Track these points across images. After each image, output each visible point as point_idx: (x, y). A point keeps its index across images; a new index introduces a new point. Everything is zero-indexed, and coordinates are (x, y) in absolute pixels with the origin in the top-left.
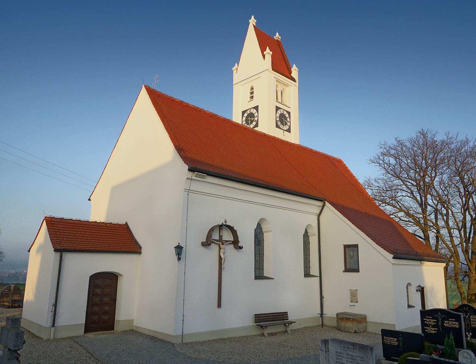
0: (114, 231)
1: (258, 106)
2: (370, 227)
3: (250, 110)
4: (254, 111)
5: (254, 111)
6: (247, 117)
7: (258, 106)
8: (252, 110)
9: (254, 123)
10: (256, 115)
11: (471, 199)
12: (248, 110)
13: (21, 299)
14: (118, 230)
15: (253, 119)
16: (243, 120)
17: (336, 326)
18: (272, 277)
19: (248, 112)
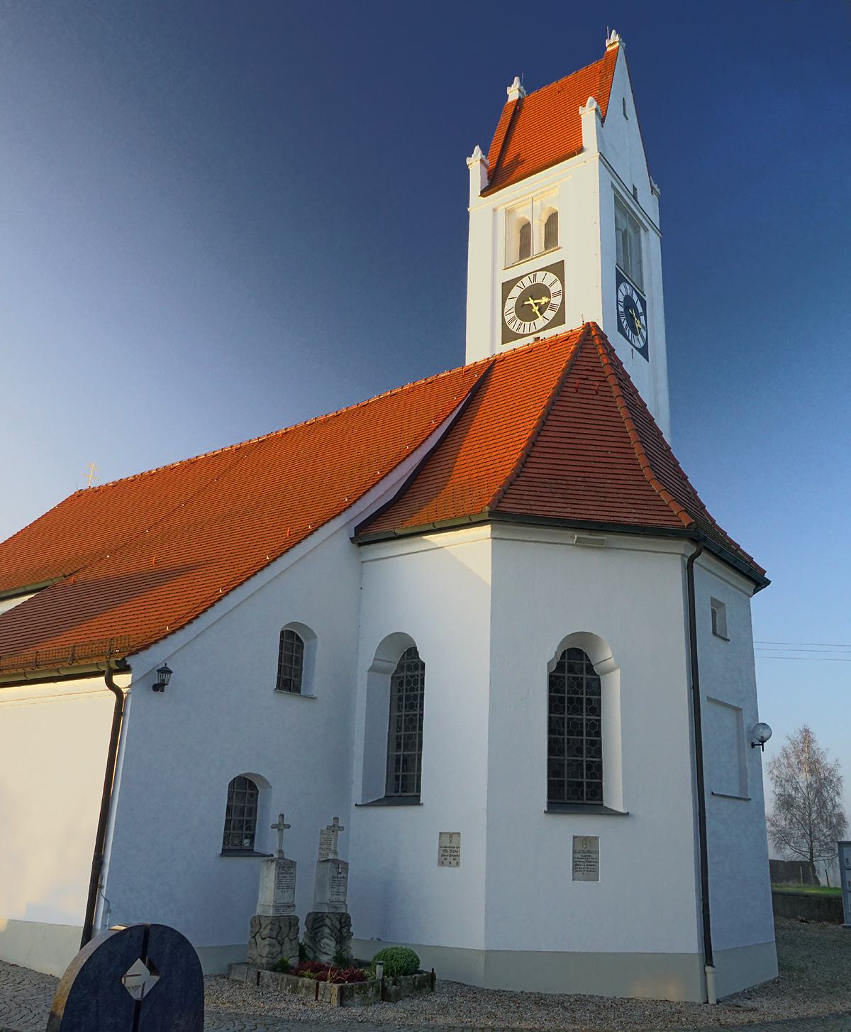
0: (550, 467)
1: (563, 261)
2: (566, 451)
3: (531, 276)
4: (549, 279)
5: (549, 279)
6: (523, 298)
7: (563, 261)
8: (540, 275)
9: (550, 314)
10: (556, 287)
11: (144, 996)
12: (522, 277)
13: (254, 805)
14: (560, 459)
15: (544, 300)
16: (507, 308)
17: (61, 977)
18: (366, 810)
19: (527, 282)
